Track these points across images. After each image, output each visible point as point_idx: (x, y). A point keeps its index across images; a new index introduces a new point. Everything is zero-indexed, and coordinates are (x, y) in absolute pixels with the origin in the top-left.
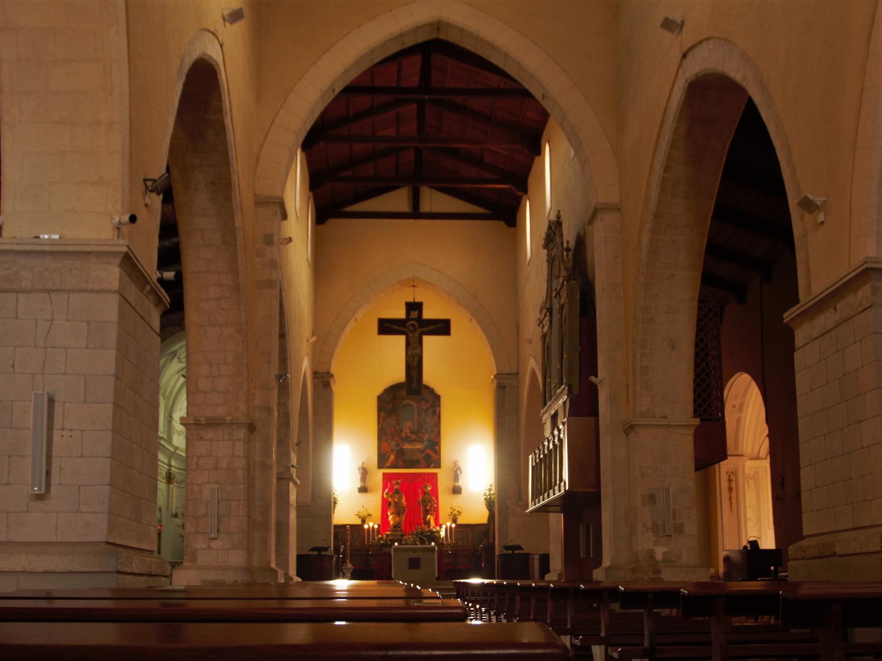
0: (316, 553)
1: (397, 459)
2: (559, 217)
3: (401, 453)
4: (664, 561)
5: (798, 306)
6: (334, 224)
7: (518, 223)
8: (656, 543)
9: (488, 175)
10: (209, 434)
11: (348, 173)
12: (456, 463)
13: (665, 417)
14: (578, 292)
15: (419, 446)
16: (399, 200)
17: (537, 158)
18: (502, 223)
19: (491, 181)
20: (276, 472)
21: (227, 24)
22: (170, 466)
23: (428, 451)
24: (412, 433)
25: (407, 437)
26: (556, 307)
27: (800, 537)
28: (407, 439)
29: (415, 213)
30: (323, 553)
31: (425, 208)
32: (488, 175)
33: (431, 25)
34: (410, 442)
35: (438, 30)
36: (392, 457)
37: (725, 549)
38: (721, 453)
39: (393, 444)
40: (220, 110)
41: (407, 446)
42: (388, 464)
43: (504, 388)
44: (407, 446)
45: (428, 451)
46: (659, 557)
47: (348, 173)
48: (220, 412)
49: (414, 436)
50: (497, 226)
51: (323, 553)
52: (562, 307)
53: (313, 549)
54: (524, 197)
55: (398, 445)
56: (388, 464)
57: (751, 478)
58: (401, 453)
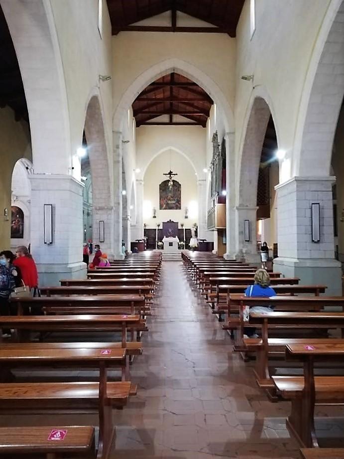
1: (166, 206)
2: (216, 133)
3: (167, 204)
4: (246, 253)
5: (279, 185)
7: (207, 126)
8: (243, 247)
9: (196, 110)
10: (100, 212)
11: (147, 110)
12: (186, 208)
13: (247, 206)
15: (174, 202)
20: (121, 225)
21: (101, 81)
22: (88, 210)
23: (177, 204)
24: (171, 197)
25: (169, 199)
27: (277, 257)
28: (169, 200)
32: (196, 110)
33: (171, 69)
34: (171, 201)
35: (174, 70)
36: (164, 206)
37: (318, 205)
39: (165, 201)
40: (99, 109)
41: (169, 202)
44: (169, 202)
46: (244, 252)
47: (147, 110)
48: (103, 205)
52: (217, 165)
53: (136, 240)
54: (208, 118)
55: (166, 202)
56: (163, 208)
58: (167, 204)
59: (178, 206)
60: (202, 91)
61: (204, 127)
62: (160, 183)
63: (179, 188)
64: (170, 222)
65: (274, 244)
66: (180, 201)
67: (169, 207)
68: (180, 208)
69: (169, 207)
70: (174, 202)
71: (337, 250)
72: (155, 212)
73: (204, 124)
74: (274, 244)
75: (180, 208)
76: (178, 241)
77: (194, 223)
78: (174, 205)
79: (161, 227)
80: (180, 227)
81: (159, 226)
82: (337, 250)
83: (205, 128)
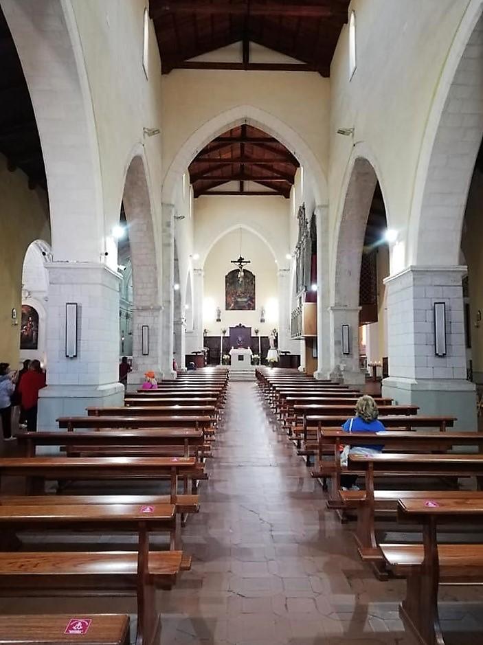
0: (195, 354)
2: (304, 205)
6: (178, 74)
11: (209, 174)
14: (311, 243)
15: (245, 300)
16: (232, 54)
17: (298, 169)
18: (316, 75)
19: (277, 178)
23: (249, 302)
26: (302, 248)
28: (239, 296)
29: (246, 65)
30: (288, 354)
31: (246, 189)
34: (241, 298)
36: (232, 305)
38: (274, 340)
41: (239, 300)
42: (230, 308)
43: (283, 276)
44: (239, 300)
45: (249, 302)
47: (209, 174)
49: (243, 295)
50: (315, 76)
51: (288, 354)
52: (304, 249)
57: (213, 358)
58: (236, 303)
59: (251, 306)
63: (252, 280)
64: (240, 327)
68: (254, 309)
70: (245, 300)
75: (254, 309)
76: (251, 353)
78: (245, 304)
79: (227, 334)
80: (253, 335)
81: (224, 332)
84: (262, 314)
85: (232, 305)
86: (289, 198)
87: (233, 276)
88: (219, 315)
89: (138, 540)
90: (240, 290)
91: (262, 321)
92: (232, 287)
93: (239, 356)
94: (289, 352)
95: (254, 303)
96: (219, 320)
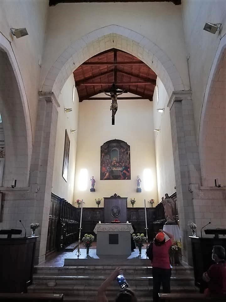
1: (109, 175)
15: (120, 169)
19: (140, 82)
28: (114, 166)
30: (13, 236)
32: (140, 80)
34: (116, 167)
36: (107, 174)
41: (114, 169)
44: (114, 169)
51: (13, 236)
58: (112, 172)
59: (126, 175)
60: (138, 61)
61: (151, 101)
62: (102, 144)
63: (127, 150)
64: (115, 197)
65: (114, 124)
66: (129, 168)
67: (113, 176)
68: (129, 178)
69: (114, 176)
70: (120, 169)
71: (69, 270)
72: (94, 182)
73: (150, 98)
74: (114, 124)
75: (129, 178)
76: (132, 231)
77: (150, 199)
78: (121, 174)
79: (101, 205)
80: (129, 206)
81: (98, 203)
82: (69, 270)
83: (151, 102)
84: (138, 184)
85: (107, 174)
86: (152, 100)
87: (108, 147)
88: (93, 185)
89: (171, 287)
90: (115, 159)
91: (139, 190)
92: (107, 157)
93: (111, 236)
94: (19, 232)
95: (129, 172)
96: (93, 190)
